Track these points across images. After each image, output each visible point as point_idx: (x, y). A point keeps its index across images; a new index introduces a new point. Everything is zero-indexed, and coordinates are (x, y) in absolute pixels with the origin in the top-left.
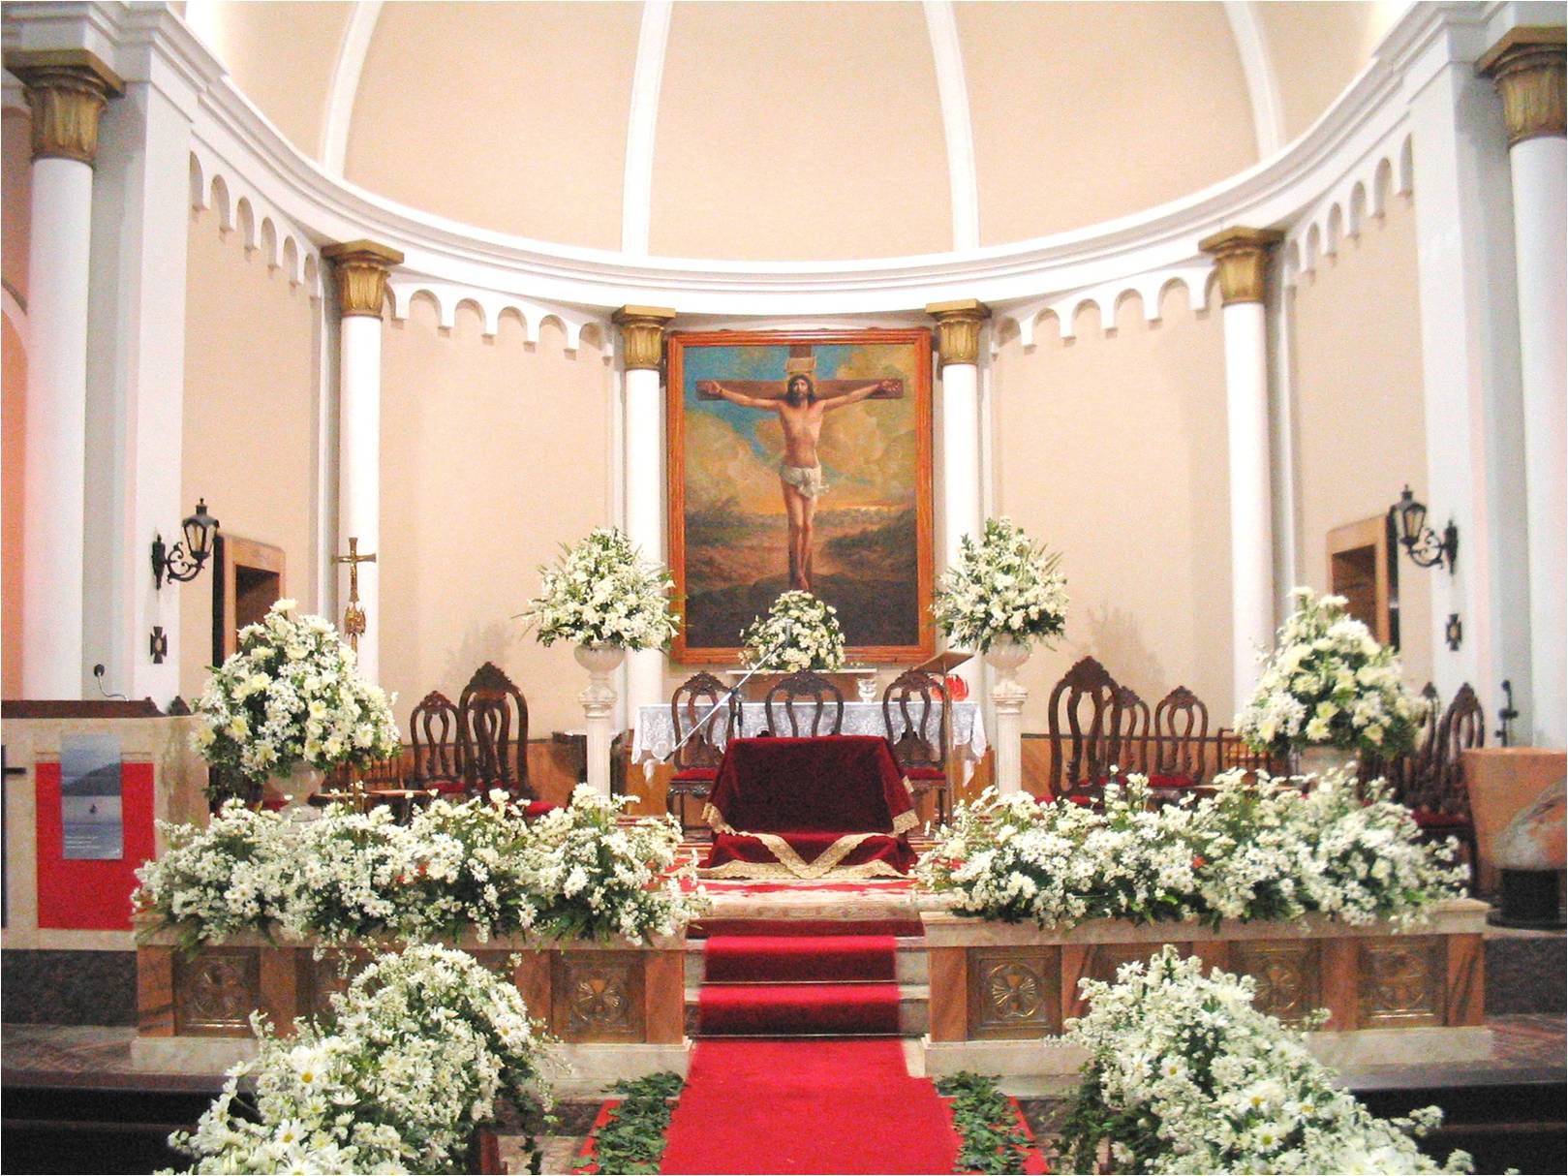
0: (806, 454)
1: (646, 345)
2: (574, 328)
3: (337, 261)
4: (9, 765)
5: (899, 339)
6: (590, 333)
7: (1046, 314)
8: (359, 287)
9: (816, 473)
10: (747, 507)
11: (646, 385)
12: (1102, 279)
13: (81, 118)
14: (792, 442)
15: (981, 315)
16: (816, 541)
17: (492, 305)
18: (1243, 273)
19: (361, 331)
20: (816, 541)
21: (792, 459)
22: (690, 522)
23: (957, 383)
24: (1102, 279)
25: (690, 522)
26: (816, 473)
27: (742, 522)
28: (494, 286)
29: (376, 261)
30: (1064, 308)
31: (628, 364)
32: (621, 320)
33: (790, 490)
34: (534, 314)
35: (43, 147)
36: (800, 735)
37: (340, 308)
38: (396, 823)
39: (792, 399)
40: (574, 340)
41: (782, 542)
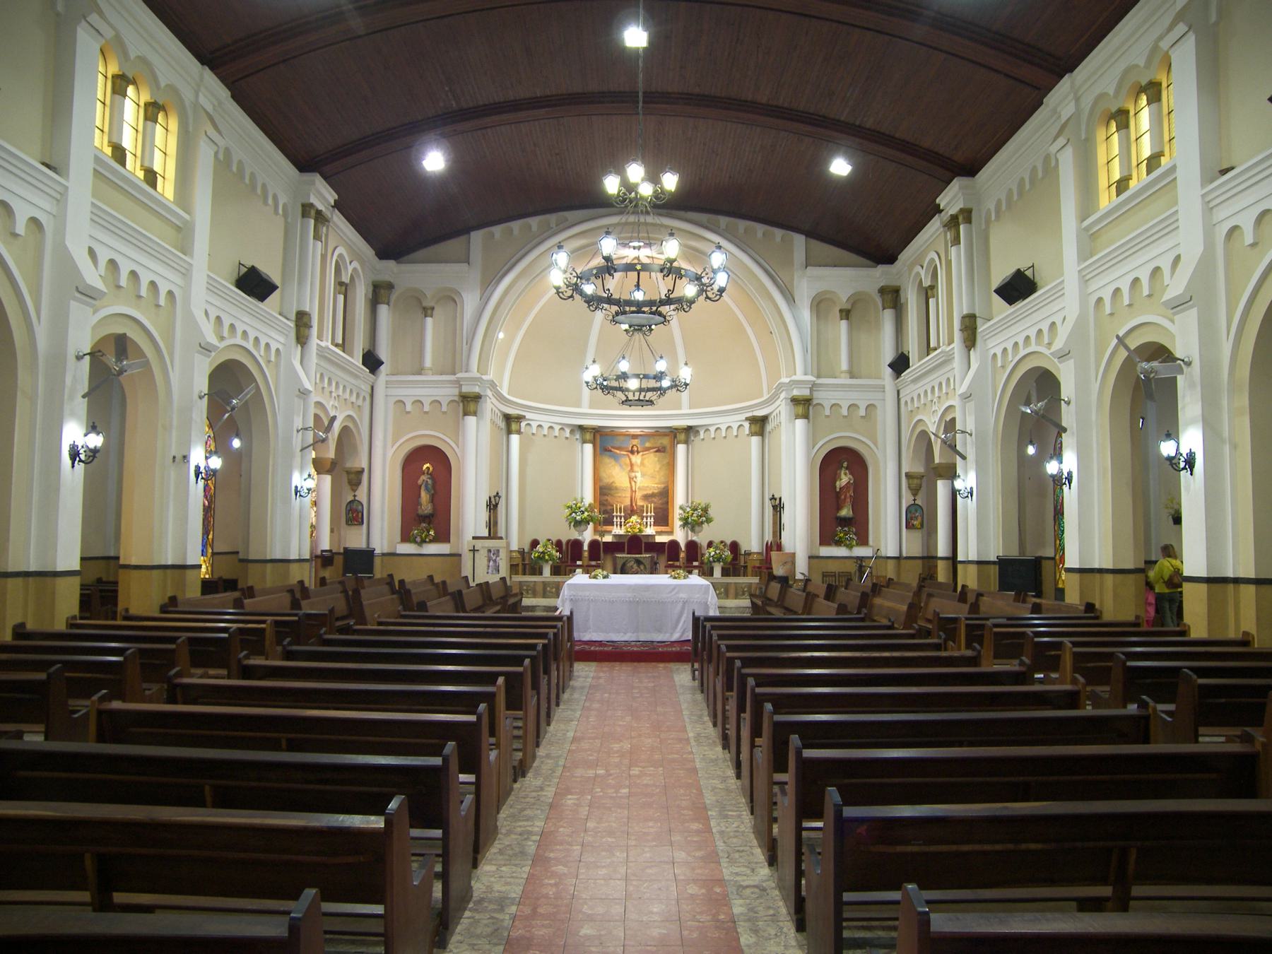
0: (636, 468)
1: (588, 436)
2: (568, 431)
3: (508, 418)
4: (487, 534)
5: (665, 435)
6: (572, 432)
7: (707, 430)
8: (514, 426)
9: (639, 475)
10: (617, 484)
11: (589, 448)
12: (723, 422)
13: (472, 407)
14: (632, 465)
15: (689, 430)
16: (639, 495)
17: (546, 426)
18: (756, 428)
19: (515, 439)
20: (639, 495)
21: (632, 470)
22: (601, 488)
23: (681, 449)
24: (723, 422)
25: (601, 488)
26: (639, 475)
27: (616, 488)
28: (546, 420)
29: (519, 418)
30: (712, 429)
31: (584, 442)
32: (581, 428)
33: (631, 479)
34: (557, 428)
35: (466, 414)
36: (83, 23)
37: (509, 432)
38: (841, 311)
39: (632, 452)
40: (568, 435)
41: (628, 495)
